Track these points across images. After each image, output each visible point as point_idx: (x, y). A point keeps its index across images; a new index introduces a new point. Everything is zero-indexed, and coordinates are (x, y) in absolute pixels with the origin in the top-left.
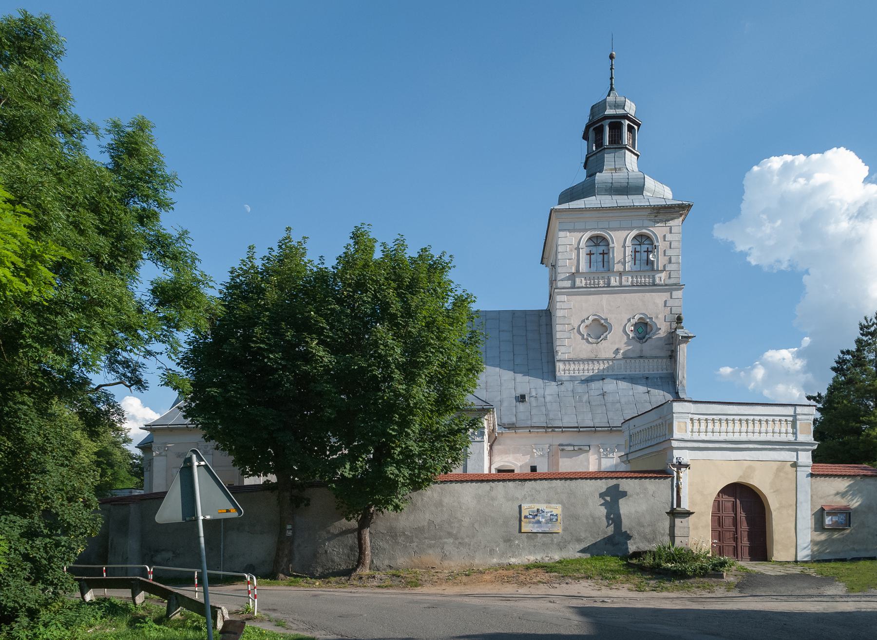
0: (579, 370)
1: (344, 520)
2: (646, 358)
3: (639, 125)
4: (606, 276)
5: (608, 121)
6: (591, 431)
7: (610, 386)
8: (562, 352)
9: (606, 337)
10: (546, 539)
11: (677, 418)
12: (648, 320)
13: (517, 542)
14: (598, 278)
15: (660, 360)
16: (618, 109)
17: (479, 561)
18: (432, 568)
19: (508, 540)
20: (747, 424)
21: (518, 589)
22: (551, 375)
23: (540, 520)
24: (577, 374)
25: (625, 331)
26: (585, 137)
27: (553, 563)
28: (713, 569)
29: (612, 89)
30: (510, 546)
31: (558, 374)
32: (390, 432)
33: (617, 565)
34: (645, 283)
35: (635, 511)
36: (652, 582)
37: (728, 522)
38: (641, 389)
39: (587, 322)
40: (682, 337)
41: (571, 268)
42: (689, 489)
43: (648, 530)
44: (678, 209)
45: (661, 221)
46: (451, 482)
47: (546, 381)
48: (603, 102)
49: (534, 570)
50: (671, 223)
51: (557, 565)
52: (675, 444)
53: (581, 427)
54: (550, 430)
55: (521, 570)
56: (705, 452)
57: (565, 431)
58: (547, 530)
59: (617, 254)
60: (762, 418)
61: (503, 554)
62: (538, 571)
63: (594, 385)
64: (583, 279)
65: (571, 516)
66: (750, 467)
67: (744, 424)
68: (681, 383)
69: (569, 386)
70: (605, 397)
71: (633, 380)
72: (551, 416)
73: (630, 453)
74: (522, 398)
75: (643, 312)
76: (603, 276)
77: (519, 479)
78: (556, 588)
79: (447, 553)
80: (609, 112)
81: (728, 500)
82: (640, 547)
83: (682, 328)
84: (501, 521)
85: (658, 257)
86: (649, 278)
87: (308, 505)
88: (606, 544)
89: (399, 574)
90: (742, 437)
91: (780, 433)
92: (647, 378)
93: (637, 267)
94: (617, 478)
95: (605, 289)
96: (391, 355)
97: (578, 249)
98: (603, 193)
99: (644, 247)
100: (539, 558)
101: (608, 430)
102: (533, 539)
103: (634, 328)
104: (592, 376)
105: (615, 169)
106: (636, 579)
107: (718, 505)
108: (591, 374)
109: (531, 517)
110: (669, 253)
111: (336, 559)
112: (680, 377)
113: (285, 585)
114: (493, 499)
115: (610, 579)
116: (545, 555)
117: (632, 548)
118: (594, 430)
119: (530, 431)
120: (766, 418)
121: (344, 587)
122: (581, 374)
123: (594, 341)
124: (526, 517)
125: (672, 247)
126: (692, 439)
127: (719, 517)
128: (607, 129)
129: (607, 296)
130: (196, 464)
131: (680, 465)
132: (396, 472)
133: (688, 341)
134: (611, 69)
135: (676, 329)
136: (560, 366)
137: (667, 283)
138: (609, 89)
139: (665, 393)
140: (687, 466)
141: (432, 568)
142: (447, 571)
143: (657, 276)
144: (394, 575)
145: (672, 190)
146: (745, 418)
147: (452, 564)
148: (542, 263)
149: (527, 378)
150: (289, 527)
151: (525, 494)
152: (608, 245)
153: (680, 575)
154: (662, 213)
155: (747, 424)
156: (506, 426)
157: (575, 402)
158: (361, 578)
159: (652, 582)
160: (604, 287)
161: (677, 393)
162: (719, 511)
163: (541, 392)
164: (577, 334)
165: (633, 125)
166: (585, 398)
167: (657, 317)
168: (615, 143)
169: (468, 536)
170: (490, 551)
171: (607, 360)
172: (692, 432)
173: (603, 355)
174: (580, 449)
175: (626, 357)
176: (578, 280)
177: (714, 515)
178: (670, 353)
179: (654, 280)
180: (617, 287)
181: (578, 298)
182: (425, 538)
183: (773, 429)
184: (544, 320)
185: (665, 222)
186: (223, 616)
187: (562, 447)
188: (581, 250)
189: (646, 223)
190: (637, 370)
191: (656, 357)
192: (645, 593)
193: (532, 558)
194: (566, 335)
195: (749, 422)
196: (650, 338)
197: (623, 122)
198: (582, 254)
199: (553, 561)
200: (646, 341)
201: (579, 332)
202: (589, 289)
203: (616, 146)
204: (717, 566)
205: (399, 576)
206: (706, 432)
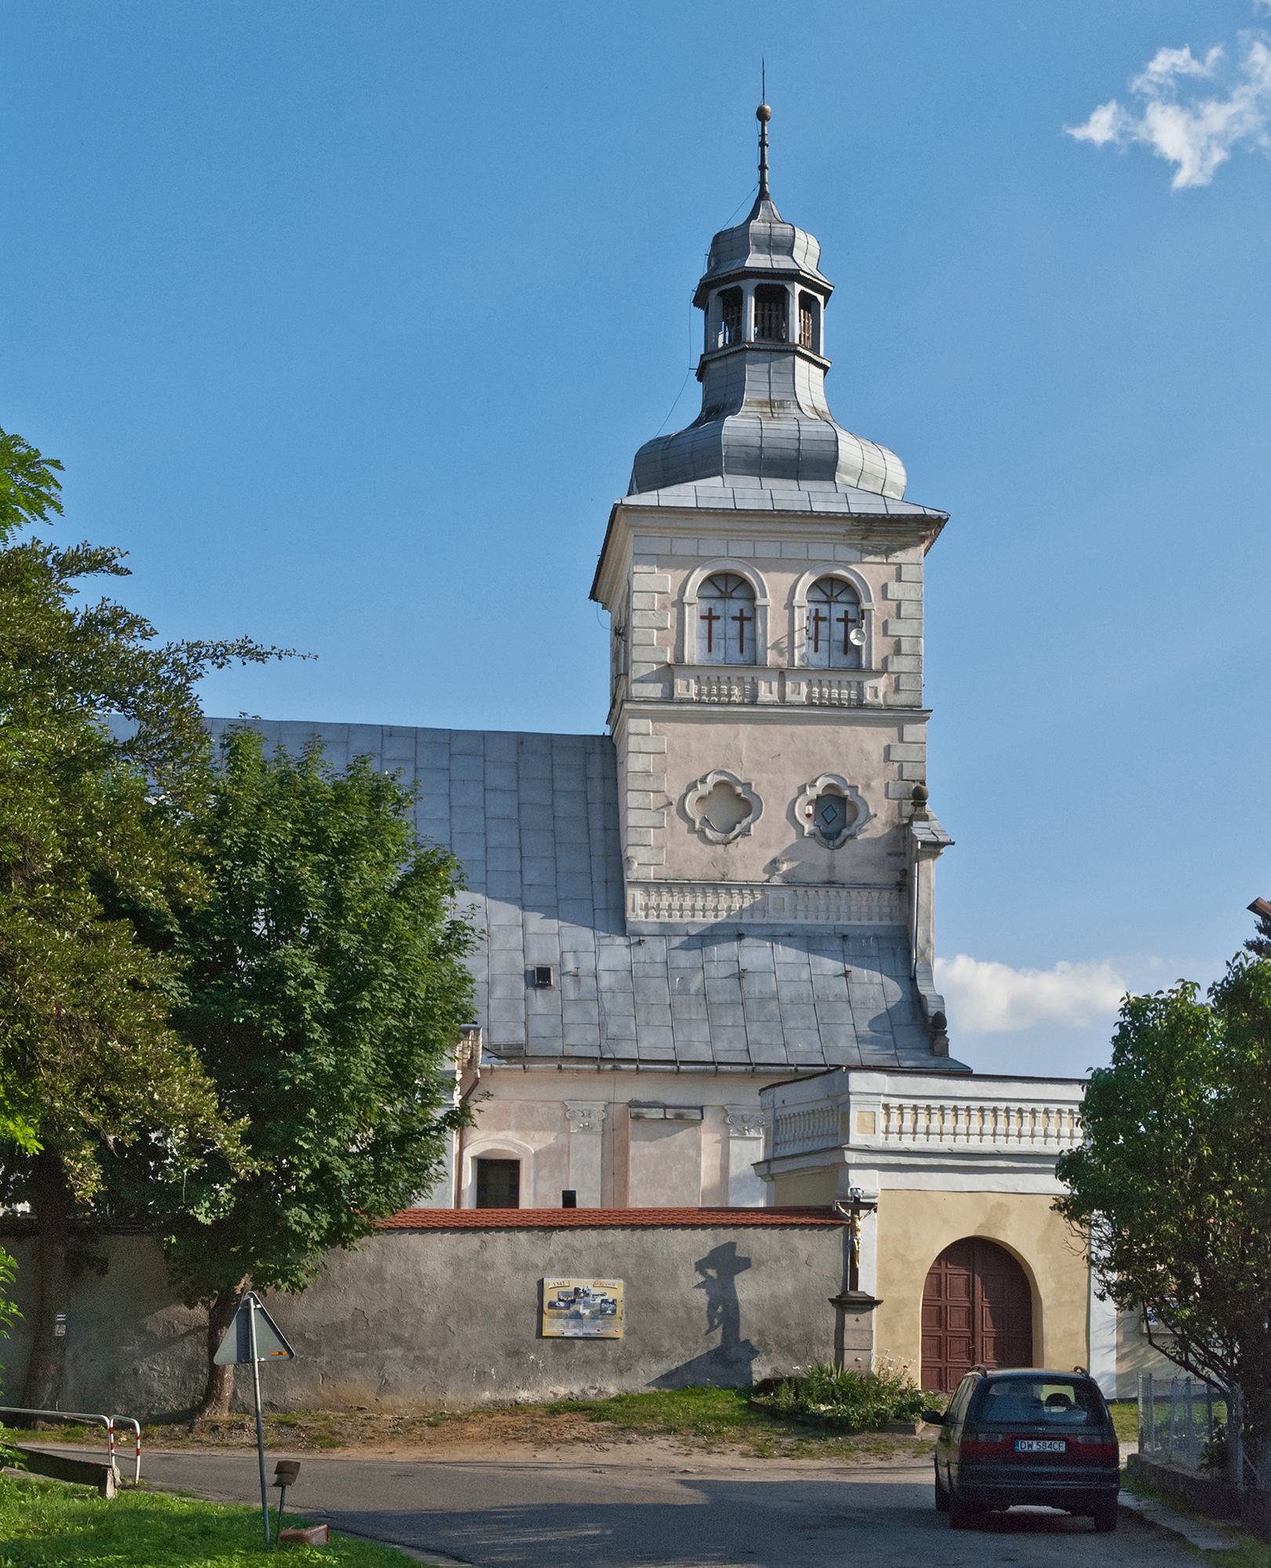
0: (681, 909)
1: (183, 1309)
2: (843, 885)
3: (827, 294)
4: (748, 675)
5: (753, 283)
6: (707, 1071)
7: (755, 954)
8: (642, 862)
10: (593, 1351)
11: (858, 1103)
12: (847, 792)
13: (532, 1357)
14: (729, 681)
15: (875, 894)
16: (776, 253)
17: (454, 1397)
18: (361, 1409)
19: (514, 1353)
20: (996, 1117)
21: (534, 1453)
22: (615, 919)
23: (581, 1311)
24: (678, 920)
26: (700, 301)
27: (603, 1401)
28: (898, 1417)
29: (763, 195)
30: (519, 1365)
31: (631, 916)
32: (301, 1143)
33: (728, 1406)
35: (772, 1295)
36: (788, 1440)
37: (957, 1321)
38: (830, 965)
39: (703, 790)
40: (924, 843)
41: (664, 652)
42: (879, 1249)
43: (795, 1334)
44: (914, 525)
46: (402, 1230)
47: (602, 934)
48: (740, 233)
49: (565, 1417)
50: (900, 557)
51: (612, 1405)
52: (851, 1157)
53: (683, 1063)
54: (610, 1066)
55: (541, 1416)
56: (912, 1175)
57: (644, 1071)
58: (593, 1332)
59: (772, 628)
60: (1023, 1106)
61: (502, 1383)
62: (574, 1417)
63: (719, 951)
64: (692, 681)
65: (642, 1304)
66: (1000, 1206)
67: (989, 1116)
68: (923, 954)
69: (657, 949)
70: (744, 983)
71: (810, 941)
72: (612, 1029)
73: (775, 1159)
74: (540, 978)
75: (835, 772)
77: (539, 1226)
78: (608, 1450)
79: (391, 1379)
80: (756, 260)
81: (957, 1276)
82: (780, 1370)
83: (925, 818)
84: (500, 1314)
85: (870, 637)
87: (103, 1272)
88: (712, 1363)
89: (293, 1421)
91: (1059, 1137)
92: (844, 937)
94: (736, 1226)
96: (308, 998)
97: (680, 604)
99: (838, 610)
100: (576, 1390)
101: (746, 1072)
102: (566, 1352)
103: (815, 810)
104: (714, 926)
105: (771, 403)
106: (759, 1434)
107: (936, 1282)
108: (712, 920)
109: (562, 1304)
110: (896, 628)
111: (157, 1387)
112: (920, 942)
113: (56, 1440)
114: (487, 1267)
115: (710, 1434)
116: (590, 1384)
117: (760, 1370)
118: (712, 1071)
119: (560, 1067)
120: (1031, 1106)
121: (185, 1447)
122: (686, 920)
123: (719, 836)
124: (552, 1305)
127: (940, 1307)
128: (751, 302)
130: (253, 1307)
131: (859, 1205)
132: (306, 1218)
133: (938, 854)
134: (762, 144)
135: (911, 819)
136: (636, 897)
137: (890, 701)
138: (756, 194)
139: (885, 978)
140: (871, 1206)
141: (361, 1409)
142: (390, 1417)
143: (869, 684)
144: (282, 1423)
145: (905, 465)
146: (991, 1105)
147: (400, 1401)
148: (593, 596)
149: (554, 924)
150: (61, 1317)
151: (551, 1258)
152: (753, 598)
153: (837, 1427)
155: (996, 1117)
156: (503, 1052)
157: (672, 993)
158: (215, 1428)
159: (787, 1441)
161: (913, 980)
162: (940, 1296)
163: (588, 961)
164: (677, 818)
166: (696, 983)
167: (868, 786)
169: (433, 1344)
170: (479, 1374)
171: (751, 887)
172: (887, 1132)
173: (741, 875)
174: (679, 1117)
175: (791, 882)
176: (680, 685)
177: (929, 1303)
180: (773, 706)
182: (347, 1347)
183: (1046, 1130)
184: (596, 768)
186: (114, 1479)
187: (636, 1110)
188: (687, 608)
189: (844, 553)
190: (822, 915)
191: (866, 886)
192: (769, 1461)
193: (562, 1391)
194: (651, 819)
195: (999, 1113)
198: (691, 634)
199: (604, 1397)
204: (905, 1410)
205: (293, 1426)
206: (915, 1133)
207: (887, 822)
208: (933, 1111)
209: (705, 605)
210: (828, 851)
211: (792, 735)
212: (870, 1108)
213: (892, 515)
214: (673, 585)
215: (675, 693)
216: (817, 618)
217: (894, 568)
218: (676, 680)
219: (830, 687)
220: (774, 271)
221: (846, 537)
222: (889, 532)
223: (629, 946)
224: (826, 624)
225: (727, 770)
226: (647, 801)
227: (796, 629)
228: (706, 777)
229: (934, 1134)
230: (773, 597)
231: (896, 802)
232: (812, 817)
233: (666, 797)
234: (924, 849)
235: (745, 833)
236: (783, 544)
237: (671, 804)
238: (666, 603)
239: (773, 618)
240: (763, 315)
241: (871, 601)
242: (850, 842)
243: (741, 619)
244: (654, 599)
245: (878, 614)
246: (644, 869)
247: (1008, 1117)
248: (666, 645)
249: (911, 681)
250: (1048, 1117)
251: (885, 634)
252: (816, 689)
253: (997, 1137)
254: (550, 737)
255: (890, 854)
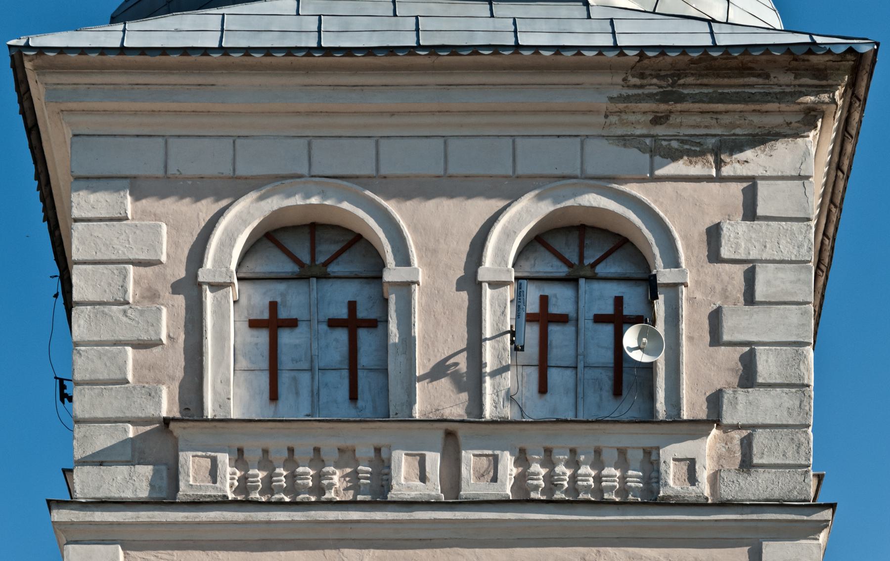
14: (317, 458)
34: (600, 490)
41: (153, 395)
44: (787, 79)
64: (224, 458)
86: (623, 463)
95: (354, 515)
154: (695, 99)
185: (717, 152)
188: (209, 297)
202: (261, 516)
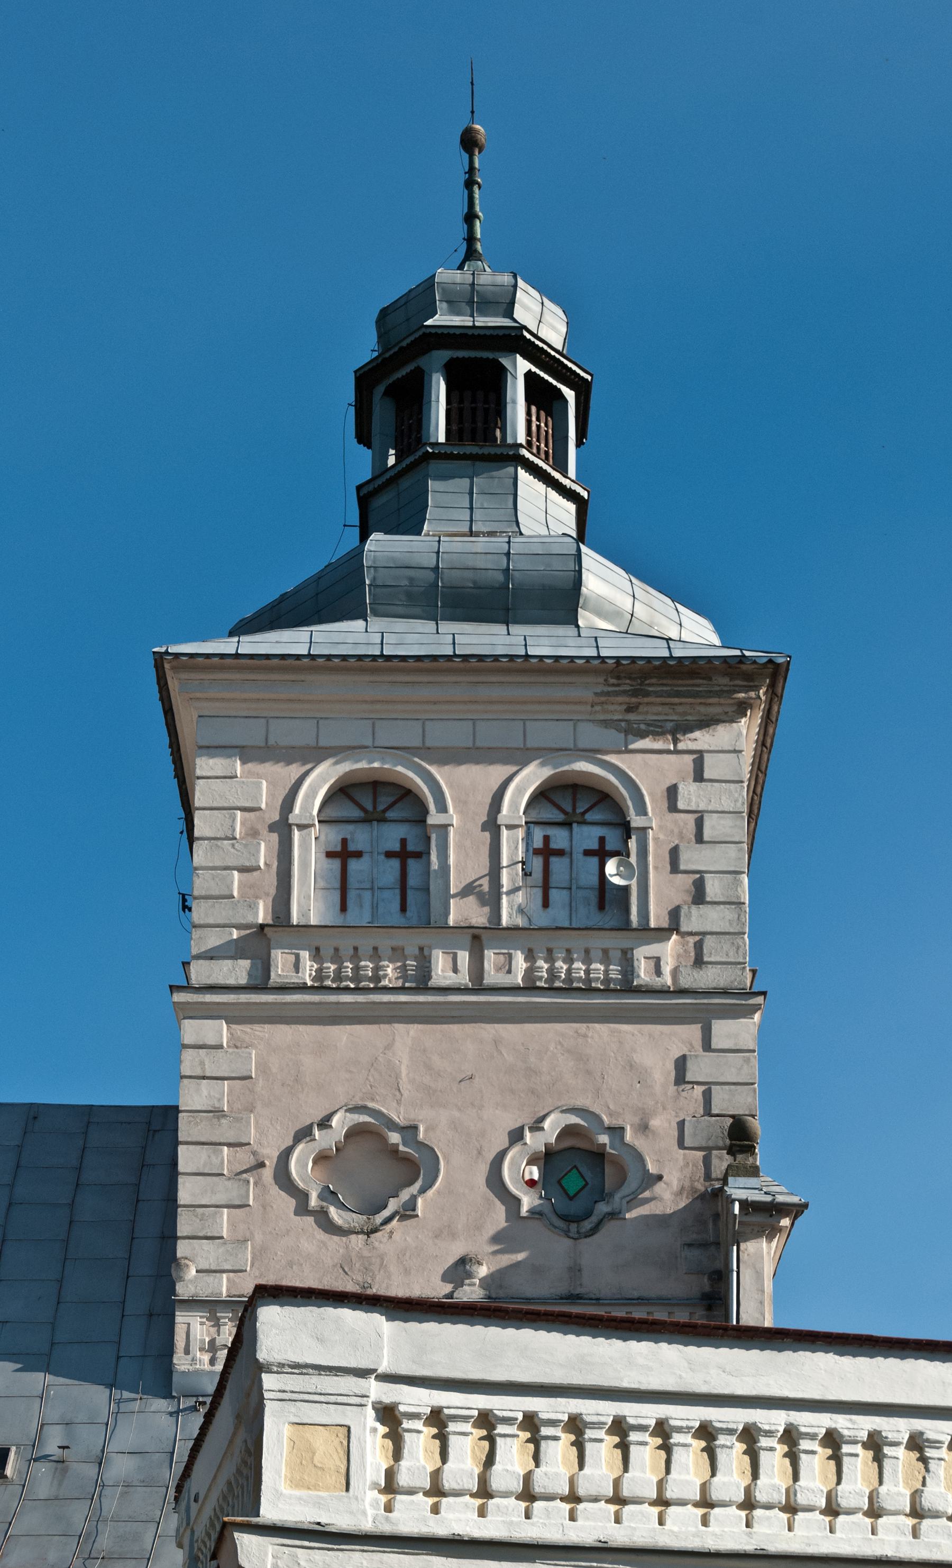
4: (411, 941)
5: (443, 356)
9: (411, 1206)
12: (604, 1139)
14: (376, 955)
20: (753, 1454)
25: (495, 1181)
31: (181, 1362)
34: (588, 980)
39: (323, 1140)
40: (744, 1204)
41: (253, 907)
44: (725, 681)
45: (655, 730)
47: (126, 1395)
50: (700, 739)
60: (841, 1422)
64: (305, 955)
75: (580, 1102)
76: (395, 943)
83: (754, 1172)
86: (606, 960)
90: (714, 1527)
93: (558, 914)
95: (403, 998)
98: (400, 610)
99: (587, 836)
103: (544, 1174)
110: (692, 858)
120: (867, 1424)
123: (356, 1220)
125: (707, 835)
126: (386, 1528)
128: (440, 389)
129: (414, 1029)
134: (470, 184)
137: (686, 982)
143: (642, 954)
146: (738, 1417)
149: (38, 1379)
154: (658, 694)
155: (753, 1454)
160: (402, 990)
164: (275, 1190)
165: (554, 382)
167: (644, 1128)
168: (473, 439)
172: (390, 1486)
178: (705, 1284)
179: (628, 969)
181: (284, 1033)
189: (590, 734)
194: (224, 1191)
196: (614, 1215)
197: (505, 362)
200: (594, 1230)
201: (283, 1178)
202: (332, 998)
203: (474, 450)
206: (484, 1492)
207: (683, 1188)
208: (545, 1431)
209: (333, 836)
210: (567, 1242)
211: (497, 1042)
212: (334, 1415)
213: (680, 659)
214: (271, 795)
215: (273, 975)
216: (547, 852)
217: (689, 759)
218: (273, 952)
219: (569, 960)
220: (476, 332)
221: (598, 708)
222: (678, 694)
223: (175, 1414)
224: (565, 861)
225: (371, 1105)
226: (215, 1160)
227: (505, 862)
228: (329, 1117)
229: (550, 1498)
230: (460, 812)
231: (701, 1154)
232: (540, 1185)
233: (254, 1153)
234: (746, 1219)
235: (408, 1212)
236: (478, 723)
237: (262, 1165)
238: (259, 827)
239: (459, 846)
240: (461, 410)
241: (646, 814)
242: (610, 1227)
243: (403, 855)
244: (234, 820)
245: (661, 836)
246: (210, 1278)
247: (793, 1457)
248: (257, 897)
249: (726, 947)
250: (924, 1460)
251: (675, 867)
252: (543, 964)
253: (758, 1513)
254: (90, 1110)
255: (690, 1245)
